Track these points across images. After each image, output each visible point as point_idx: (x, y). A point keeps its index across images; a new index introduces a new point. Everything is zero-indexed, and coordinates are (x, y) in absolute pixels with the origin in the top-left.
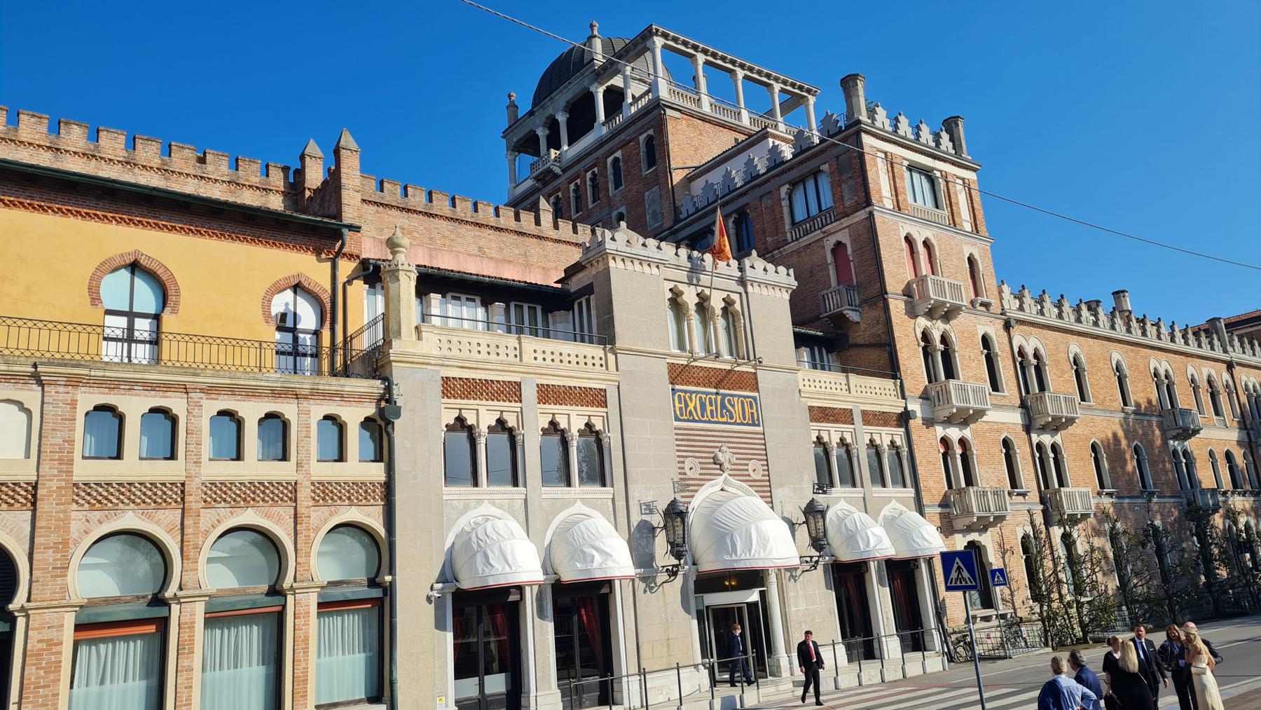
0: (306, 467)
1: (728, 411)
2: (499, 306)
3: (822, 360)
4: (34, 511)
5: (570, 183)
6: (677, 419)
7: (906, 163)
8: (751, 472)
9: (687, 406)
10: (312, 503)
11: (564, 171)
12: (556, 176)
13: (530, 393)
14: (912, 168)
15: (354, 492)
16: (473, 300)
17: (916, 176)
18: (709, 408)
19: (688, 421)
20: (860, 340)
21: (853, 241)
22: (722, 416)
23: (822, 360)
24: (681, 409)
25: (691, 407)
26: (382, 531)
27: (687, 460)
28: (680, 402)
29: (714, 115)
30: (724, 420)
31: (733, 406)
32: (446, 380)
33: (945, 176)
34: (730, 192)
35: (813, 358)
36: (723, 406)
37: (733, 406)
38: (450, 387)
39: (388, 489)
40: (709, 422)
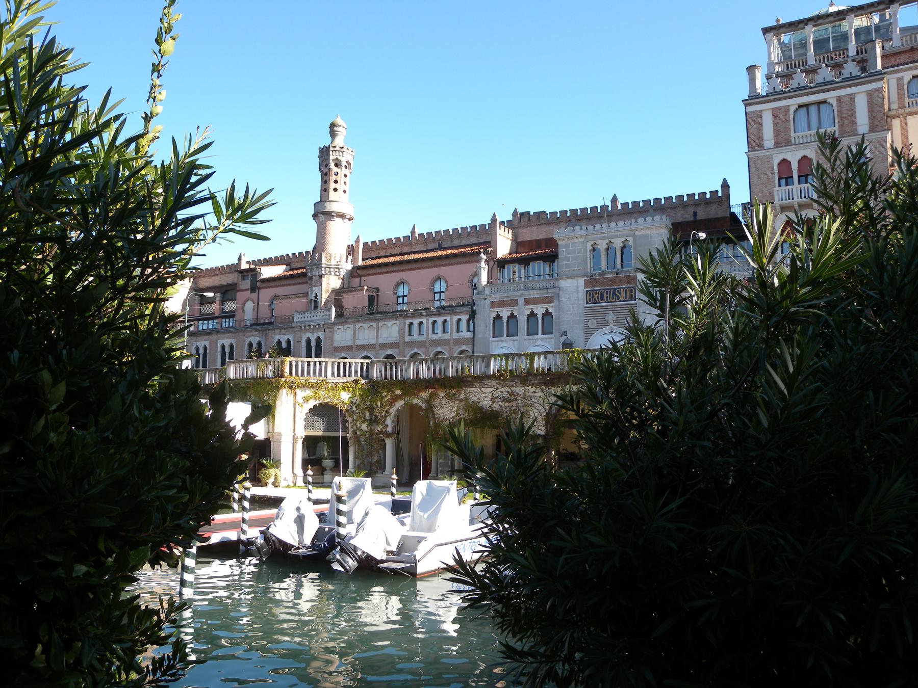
13: (521, 301)
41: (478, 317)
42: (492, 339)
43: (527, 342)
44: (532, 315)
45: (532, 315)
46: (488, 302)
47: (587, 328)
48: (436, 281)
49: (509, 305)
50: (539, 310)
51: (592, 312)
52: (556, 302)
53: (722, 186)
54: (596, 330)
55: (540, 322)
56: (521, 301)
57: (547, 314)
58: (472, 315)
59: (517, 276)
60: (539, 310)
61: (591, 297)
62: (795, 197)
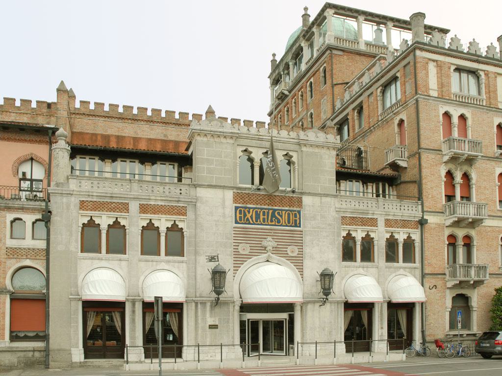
0: (3, 241)
1: (277, 218)
2: (370, 186)
3: (384, 191)
4: (137, 362)
5: (292, 99)
6: (236, 222)
7: (453, 68)
8: (288, 252)
9: (245, 215)
10: (6, 257)
11: (290, 92)
12: (286, 96)
13: (134, 206)
14: (459, 70)
15: (31, 253)
16: (359, 182)
17: (464, 76)
18: (262, 217)
19: (245, 224)
20: (407, 179)
21: (408, 118)
22: (272, 221)
23: (384, 191)
24: (240, 218)
25: (249, 216)
26: (44, 272)
27: (241, 245)
28: (240, 213)
29: (368, 51)
30: (273, 223)
31: (281, 216)
32: (82, 202)
33: (487, 74)
34: (351, 98)
35: (377, 191)
36: (273, 215)
37: (281, 216)
38: (83, 205)
39: (48, 250)
40: (261, 224)
41: (54, 218)
42: (80, 254)
43: (142, 264)
44: (150, 228)
45: (150, 228)
46: (74, 201)
47: (236, 253)
48: (26, 161)
49: (113, 210)
50: (163, 223)
51: (241, 236)
52: (190, 214)
53: (207, 113)
54: (249, 256)
55: (163, 239)
56: (134, 206)
57: (174, 229)
58: (46, 218)
59: (472, 145)
60: (163, 223)
61: (241, 216)
62: (471, 214)
